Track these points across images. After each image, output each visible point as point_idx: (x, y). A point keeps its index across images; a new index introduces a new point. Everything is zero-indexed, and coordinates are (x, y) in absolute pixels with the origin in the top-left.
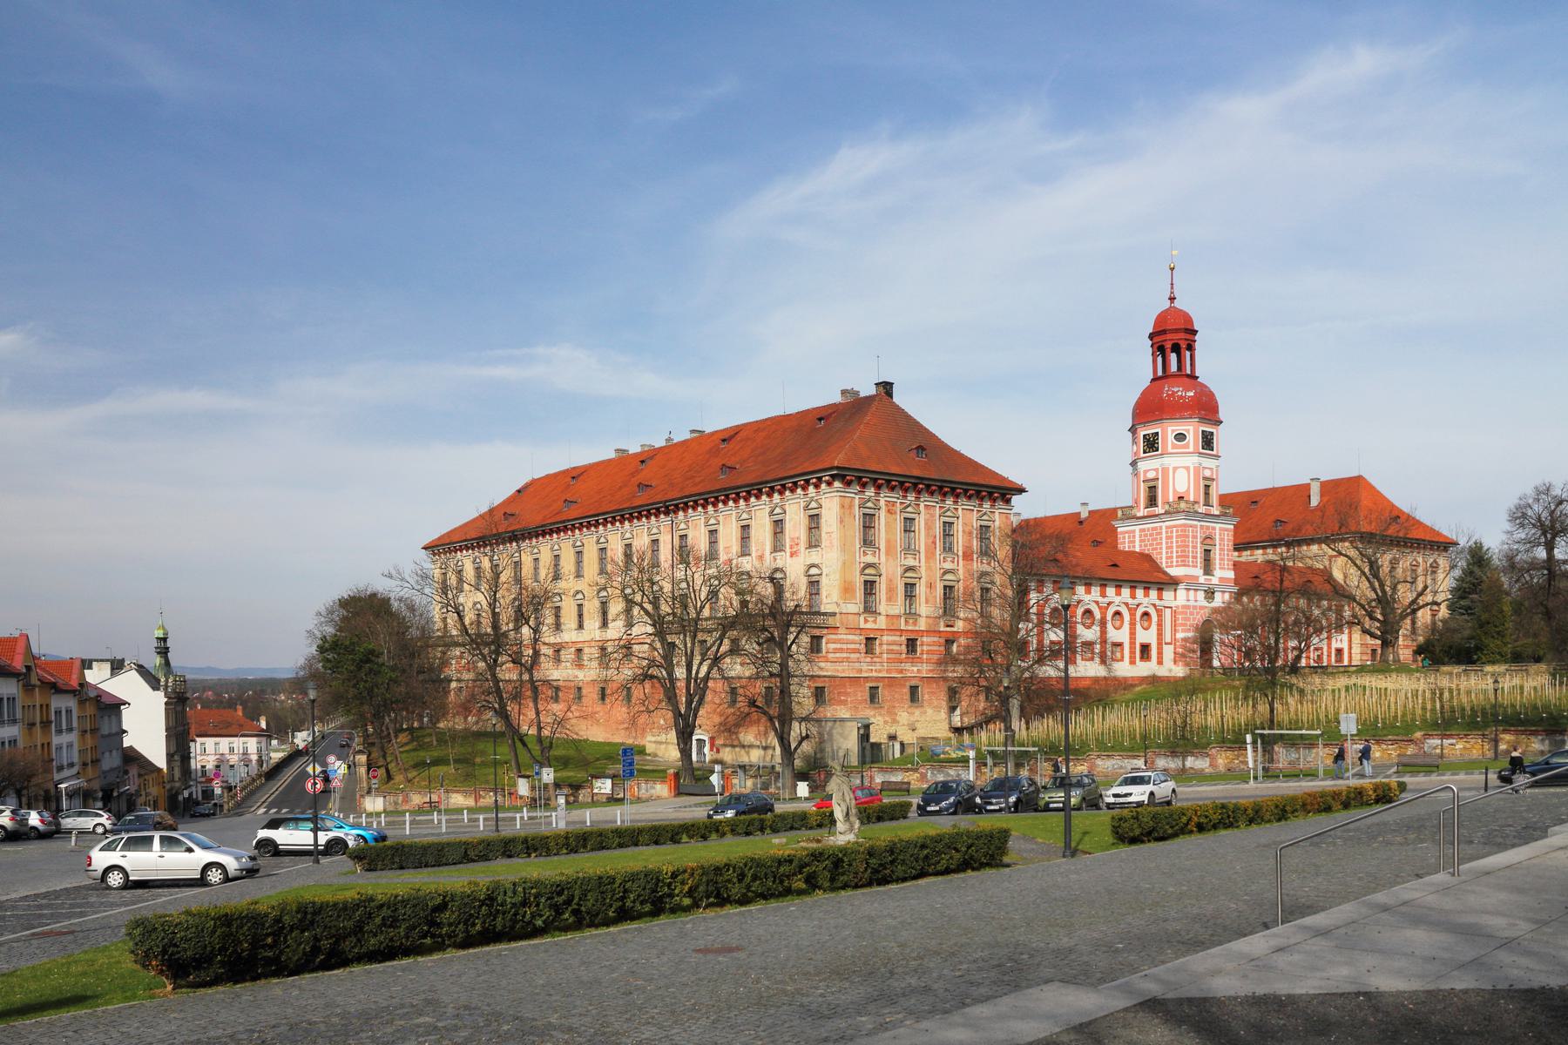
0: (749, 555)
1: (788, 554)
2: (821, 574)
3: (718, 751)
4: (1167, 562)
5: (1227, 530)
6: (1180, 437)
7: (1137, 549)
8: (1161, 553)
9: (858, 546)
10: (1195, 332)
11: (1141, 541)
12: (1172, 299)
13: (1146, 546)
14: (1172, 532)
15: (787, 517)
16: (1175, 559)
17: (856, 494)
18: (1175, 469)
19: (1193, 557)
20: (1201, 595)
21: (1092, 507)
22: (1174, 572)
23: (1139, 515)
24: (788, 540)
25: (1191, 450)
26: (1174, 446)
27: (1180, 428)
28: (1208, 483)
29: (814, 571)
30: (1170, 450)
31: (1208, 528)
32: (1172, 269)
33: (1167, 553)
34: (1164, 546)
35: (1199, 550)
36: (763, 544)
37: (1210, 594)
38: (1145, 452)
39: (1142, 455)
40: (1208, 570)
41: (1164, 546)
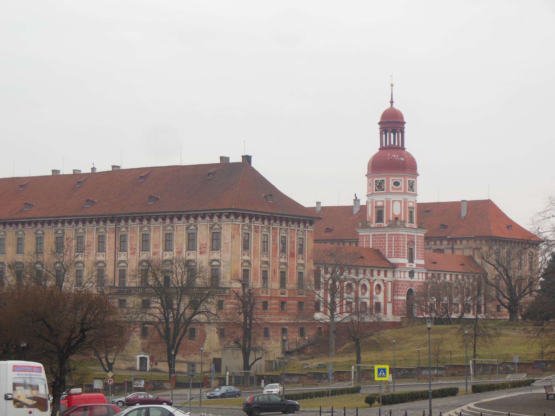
0: (172, 250)
1: (198, 253)
2: (220, 265)
3: (156, 364)
4: (388, 255)
5: (421, 237)
6: (396, 184)
7: (371, 247)
8: (385, 249)
9: (241, 250)
10: (405, 123)
11: (373, 241)
12: (392, 102)
13: (376, 244)
14: (392, 238)
15: (198, 232)
16: (393, 254)
17: (240, 222)
18: (394, 201)
19: (403, 252)
20: (407, 275)
21: (322, 205)
22: (393, 260)
23: (372, 226)
24: (198, 245)
25: (403, 191)
26: (393, 189)
27: (397, 179)
28: (411, 210)
29: (215, 263)
30: (391, 191)
31: (411, 236)
32: (392, 85)
33: (389, 249)
34: (387, 245)
35: (406, 248)
36: (182, 245)
37: (411, 274)
38: (376, 190)
39: (375, 192)
40: (411, 260)
41: (387, 245)
